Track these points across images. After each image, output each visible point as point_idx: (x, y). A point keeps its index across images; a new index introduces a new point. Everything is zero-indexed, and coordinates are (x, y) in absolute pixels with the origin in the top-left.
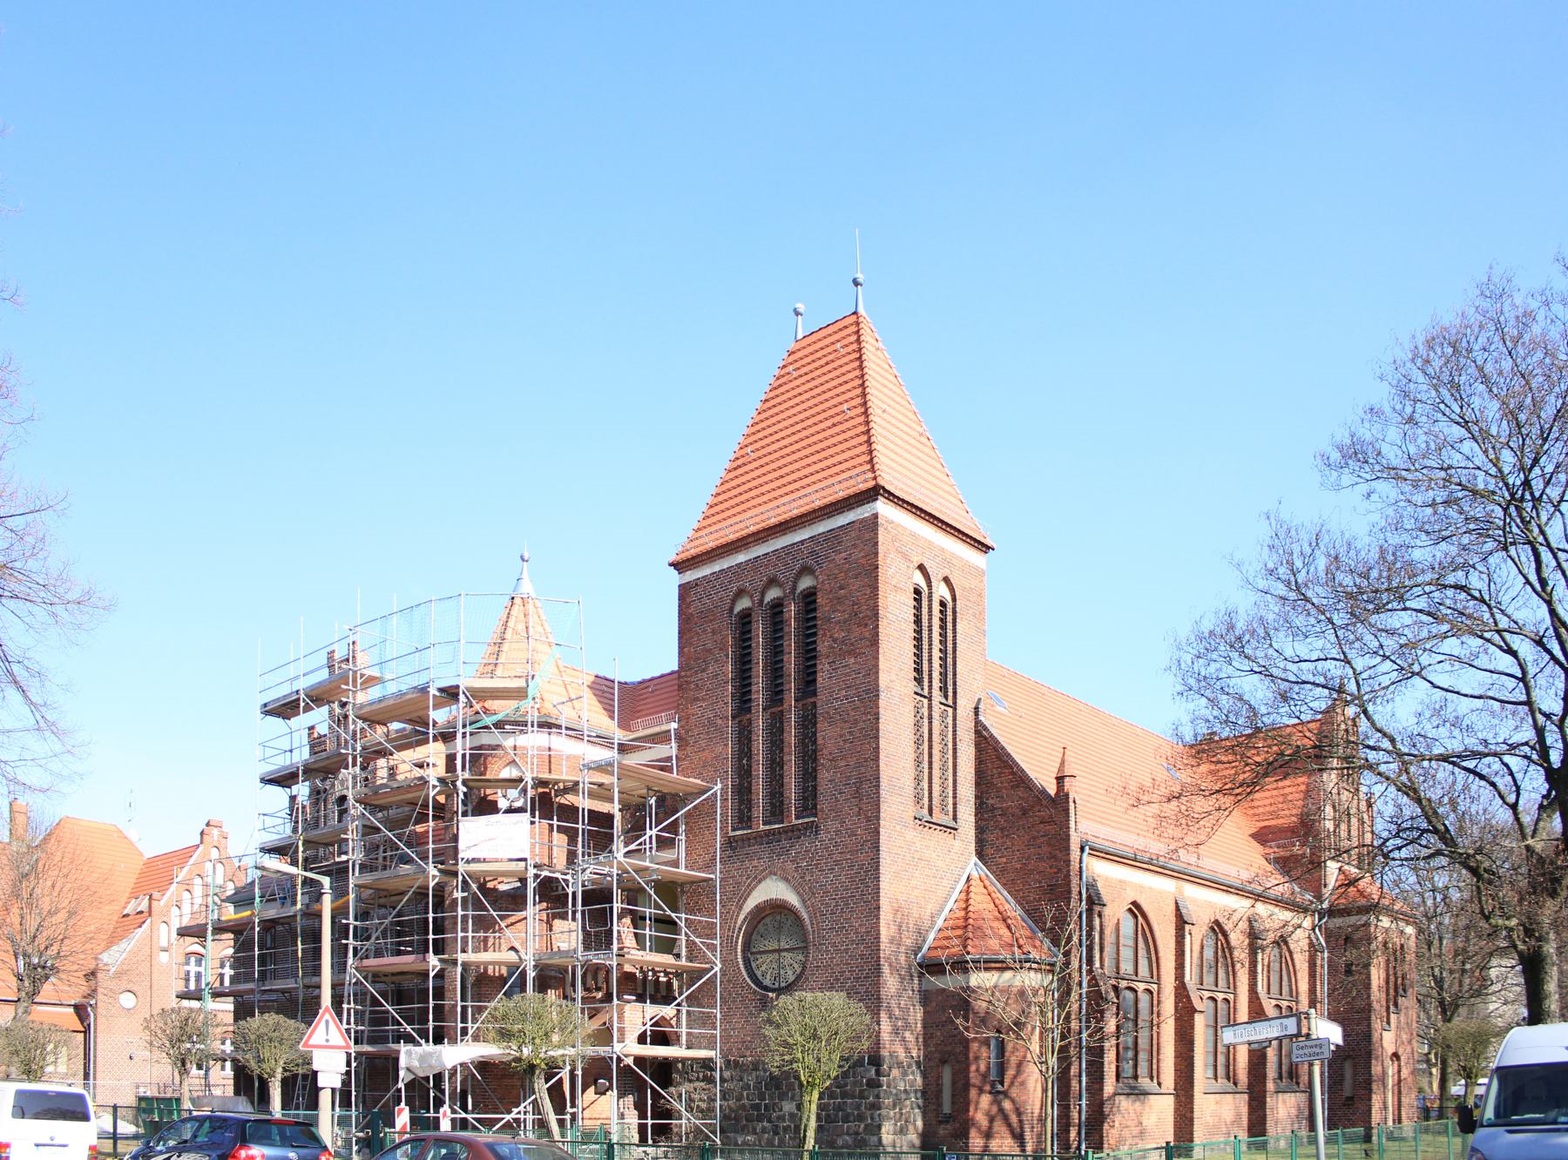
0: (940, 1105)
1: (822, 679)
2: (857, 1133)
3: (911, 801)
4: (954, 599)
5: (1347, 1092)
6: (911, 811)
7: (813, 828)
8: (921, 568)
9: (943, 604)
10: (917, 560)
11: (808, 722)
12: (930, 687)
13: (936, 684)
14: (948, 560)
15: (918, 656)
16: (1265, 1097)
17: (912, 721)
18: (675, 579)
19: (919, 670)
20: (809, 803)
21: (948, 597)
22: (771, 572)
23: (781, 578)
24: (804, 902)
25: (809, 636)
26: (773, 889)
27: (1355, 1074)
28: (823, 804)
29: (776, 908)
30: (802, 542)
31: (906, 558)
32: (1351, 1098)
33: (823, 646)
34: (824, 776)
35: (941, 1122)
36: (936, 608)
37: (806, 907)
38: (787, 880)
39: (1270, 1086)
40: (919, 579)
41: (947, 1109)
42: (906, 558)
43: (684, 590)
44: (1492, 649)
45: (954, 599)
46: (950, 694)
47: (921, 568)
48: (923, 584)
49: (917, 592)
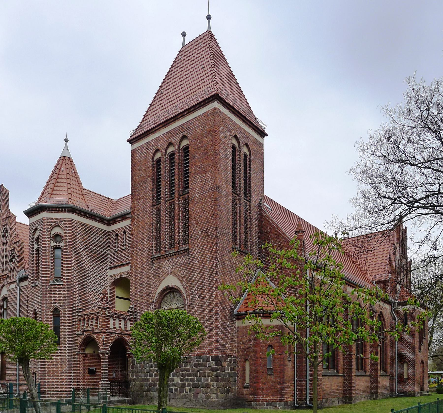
0: (244, 379)
1: (191, 184)
2: (207, 393)
3: (231, 240)
4: (250, 154)
5: (405, 376)
6: (231, 245)
7: (187, 251)
8: (235, 137)
9: (245, 156)
10: (234, 133)
11: (186, 204)
12: (240, 191)
13: (242, 189)
14: (248, 136)
15: (234, 176)
16: (377, 378)
17: (231, 204)
18: (129, 147)
19: (234, 183)
20: (186, 239)
21: (248, 153)
22: (170, 140)
23: (174, 142)
24: (183, 286)
25: (186, 184)
26: (171, 281)
27: (408, 369)
28: (192, 240)
29: (171, 290)
30: (183, 125)
31: (229, 130)
32: (407, 378)
33: (191, 170)
34: (192, 228)
35: (245, 388)
36: (242, 157)
37: (184, 288)
38: (176, 276)
39: (379, 373)
40: (234, 142)
41: (247, 381)
42: (229, 130)
43: (133, 152)
44: (419, 217)
45: (250, 154)
46: (249, 196)
47: (235, 137)
48: (236, 145)
49: (234, 147)
